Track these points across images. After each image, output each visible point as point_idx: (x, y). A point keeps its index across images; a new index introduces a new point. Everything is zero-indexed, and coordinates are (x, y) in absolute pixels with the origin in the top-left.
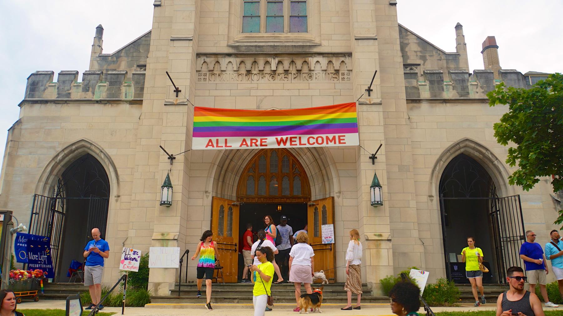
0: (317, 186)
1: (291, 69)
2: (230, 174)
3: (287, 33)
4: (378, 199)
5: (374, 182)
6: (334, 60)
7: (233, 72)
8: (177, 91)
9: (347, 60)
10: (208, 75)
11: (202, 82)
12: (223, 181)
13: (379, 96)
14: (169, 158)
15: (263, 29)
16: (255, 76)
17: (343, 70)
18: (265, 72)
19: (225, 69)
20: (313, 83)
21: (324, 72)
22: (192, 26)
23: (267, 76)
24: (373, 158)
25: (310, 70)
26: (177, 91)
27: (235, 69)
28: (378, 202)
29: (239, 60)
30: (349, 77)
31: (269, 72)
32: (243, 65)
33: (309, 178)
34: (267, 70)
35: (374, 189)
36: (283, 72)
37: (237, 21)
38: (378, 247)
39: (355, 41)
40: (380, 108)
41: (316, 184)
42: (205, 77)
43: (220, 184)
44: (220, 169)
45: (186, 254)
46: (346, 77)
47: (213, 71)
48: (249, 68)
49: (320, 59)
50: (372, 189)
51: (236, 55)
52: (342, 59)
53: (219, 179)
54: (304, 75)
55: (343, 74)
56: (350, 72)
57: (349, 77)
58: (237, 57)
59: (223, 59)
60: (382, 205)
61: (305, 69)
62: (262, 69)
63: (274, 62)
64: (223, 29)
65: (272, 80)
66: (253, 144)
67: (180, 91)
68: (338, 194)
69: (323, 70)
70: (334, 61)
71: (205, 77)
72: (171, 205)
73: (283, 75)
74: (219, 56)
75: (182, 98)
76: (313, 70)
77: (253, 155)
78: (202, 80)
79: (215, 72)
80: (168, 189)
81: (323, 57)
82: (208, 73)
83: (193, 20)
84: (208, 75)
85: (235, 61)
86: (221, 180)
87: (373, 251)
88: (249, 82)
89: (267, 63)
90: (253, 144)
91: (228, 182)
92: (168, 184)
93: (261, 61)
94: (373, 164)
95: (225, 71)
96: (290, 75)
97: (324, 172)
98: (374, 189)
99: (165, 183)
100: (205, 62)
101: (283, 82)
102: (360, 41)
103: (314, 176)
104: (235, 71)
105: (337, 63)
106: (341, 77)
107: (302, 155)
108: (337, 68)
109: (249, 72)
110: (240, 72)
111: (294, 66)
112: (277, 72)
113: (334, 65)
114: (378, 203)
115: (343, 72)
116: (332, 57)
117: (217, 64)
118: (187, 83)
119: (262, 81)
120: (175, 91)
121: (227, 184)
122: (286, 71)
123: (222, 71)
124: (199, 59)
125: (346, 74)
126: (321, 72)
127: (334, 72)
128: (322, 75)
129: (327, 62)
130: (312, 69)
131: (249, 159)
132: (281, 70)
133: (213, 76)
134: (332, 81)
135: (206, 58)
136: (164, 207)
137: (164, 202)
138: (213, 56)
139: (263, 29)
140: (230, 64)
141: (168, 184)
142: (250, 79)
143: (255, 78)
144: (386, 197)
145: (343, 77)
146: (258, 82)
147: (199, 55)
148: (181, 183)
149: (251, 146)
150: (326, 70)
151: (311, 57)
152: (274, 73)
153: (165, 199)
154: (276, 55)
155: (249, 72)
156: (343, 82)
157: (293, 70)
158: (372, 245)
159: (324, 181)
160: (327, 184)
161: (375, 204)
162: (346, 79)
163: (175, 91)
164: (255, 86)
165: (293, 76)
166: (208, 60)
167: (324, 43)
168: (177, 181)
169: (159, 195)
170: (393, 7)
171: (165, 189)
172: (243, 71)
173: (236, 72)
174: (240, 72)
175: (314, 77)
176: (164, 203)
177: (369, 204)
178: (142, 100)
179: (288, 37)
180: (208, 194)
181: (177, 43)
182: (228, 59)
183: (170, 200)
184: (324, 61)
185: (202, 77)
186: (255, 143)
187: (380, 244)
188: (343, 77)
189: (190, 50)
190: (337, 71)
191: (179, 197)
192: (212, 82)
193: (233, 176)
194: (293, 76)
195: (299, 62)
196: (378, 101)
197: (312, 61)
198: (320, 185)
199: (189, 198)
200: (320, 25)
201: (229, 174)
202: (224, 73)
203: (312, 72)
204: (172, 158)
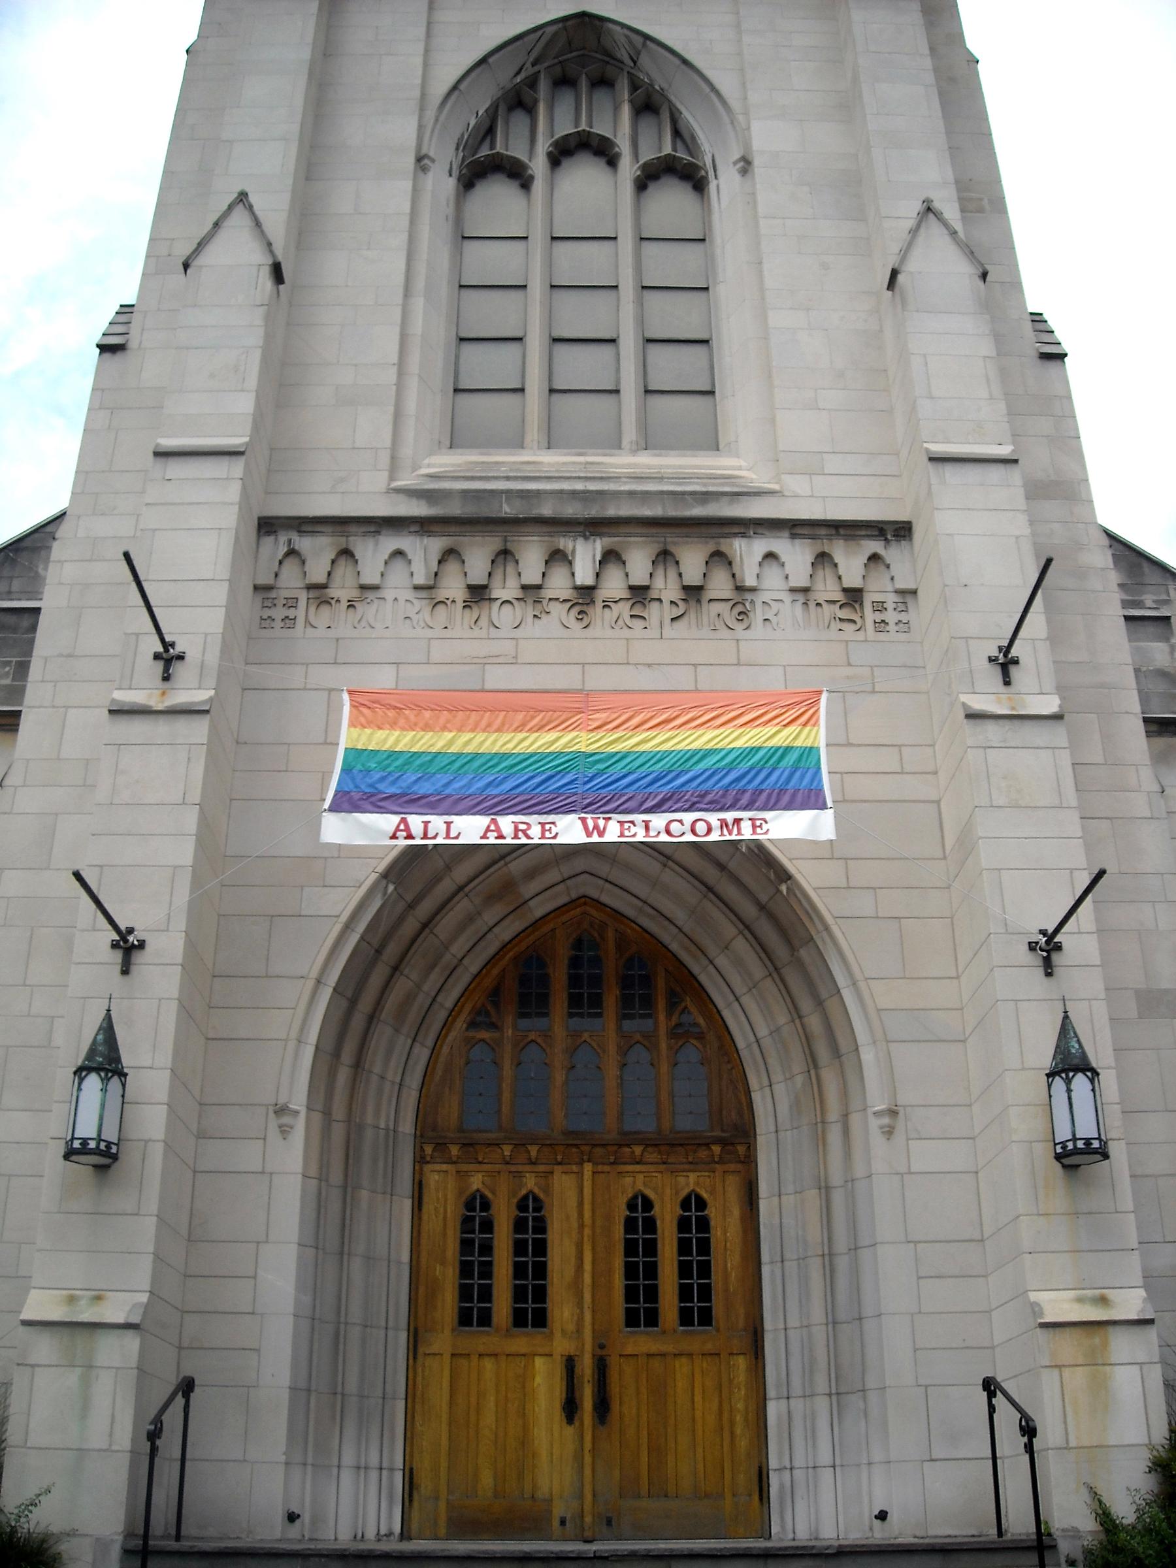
0: (779, 1089)
1: (659, 583)
2: (389, 1031)
3: (634, 452)
4: (1086, 1129)
5: (1062, 1049)
6: (839, 551)
7: (410, 594)
8: (168, 659)
9: (893, 554)
10: (302, 603)
11: (278, 631)
12: (358, 1065)
13: (1049, 684)
14: (115, 945)
15: (533, 433)
16: (507, 607)
17: (878, 589)
18: (548, 593)
19: (376, 580)
20: (756, 639)
21: (801, 598)
22: (245, 404)
23: (558, 610)
24: (1048, 949)
25: (740, 589)
26: (168, 659)
27: (420, 580)
28: (1088, 1142)
29: (436, 545)
30: (903, 617)
31: (567, 594)
32: (452, 567)
33: (744, 1054)
34: (559, 585)
35: (1068, 1082)
36: (625, 594)
37: (425, 403)
38: (1097, 1361)
39: (929, 464)
40: (1058, 735)
41: (777, 1076)
42: (291, 613)
43: (343, 1076)
44: (344, 1004)
45: (180, 1401)
46: (891, 616)
47: (324, 587)
48: (478, 578)
49: (781, 545)
50: (1058, 1083)
51: (423, 526)
52: (875, 546)
53: (337, 1054)
54: (717, 608)
55: (880, 607)
56: (909, 599)
57: (903, 617)
58: (430, 534)
59: (370, 542)
60: (1106, 1156)
61: (720, 585)
62: (537, 580)
63: (585, 556)
64: (371, 426)
65: (576, 626)
66: (520, 834)
67: (181, 657)
68: (886, 1120)
69: (793, 590)
70: (838, 557)
71: (291, 613)
72: (115, 1157)
73: (624, 609)
74: (353, 528)
75: (190, 690)
76: (753, 590)
77: (492, 950)
78: (278, 624)
79: (333, 592)
80: (106, 1081)
81: (793, 536)
82: (303, 596)
83: (252, 382)
84: (302, 603)
85: (422, 551)
86: (347, 1057)
87: (1077, 1378)
88: (476, 632)
89: (557, 557)
90: (520, 834)
91: (377, 1069)
92: (105, 1060)
93: (531, 559)
94: (1049, 974)
95: (376, 588)
96: (655, 606)
97: (814, 1022)
98: (1068, 1082)
99: (92, 1052)
100: (292, 552)
101: (626, 633)
102: (949, 469)
103: (767, 1042)
104: (417, 588)
105: (851, 564)
106: (870, 616)
107: (712, 951)
108: (853, 579)
109: (478, 594)
110: (441, 594)
111: (672, 574)
112: (602, 594)
113: (841, 571)
114: (1088, 1150)
115: (879, 597)
116: (830, 537)
117: (342, 562)
118: (213, 621)
119: (532, 629)
120: (157, 657)
121: (374, 1079)
122: (640, 594)
123: (363, 587)
124: (268, 541)
125: (890, 606)
126: (787, 597)
127: (839, 596)
128: (790, 611)
129: (809, 558)
130: (750, 581)
131: (474, 969)
132: (614, 585)
133: (325, 609)
134: (833, 634)
135: (295, 536)
136: (81, 1170)
137: (85, 1142)
138: (328, 529)
139: (533, 433)
140: (399, 564)
141: (105, 1060)
142: (484, 621)
143: (505, 616)
144: (1114, 1128)
145: (879, 617)
146: (518, 633)
147: (267, 526)
148: (165, 1058)
149: (516, 837)
150: (806, 590)
151: (743, 535)
152: (585, 596)
153: (87, 1129)
154: (593, 527)
155: (478, 594)
156: (882, 636)
157: (667, 587)
158: (1068, 1346)
159: (813, 1061)
160: (829, 1078)
161: (1076, 1151)
162: (892, 627)
163: (157, 657)
164: (508, 647)
165: (669, 612)
166: (304, 544)
167: (796, 484)
168: (148, 1053)
169: (61, 1111)
170: (1052, 365)
171: (93, 1082)
172: (453, 587)
173: (424, 594)
174: (441, 594)
175: (758, 614)
176: (84, 1150)
177: (1044, 1154)
178: (18, 714)
179: (636, 468)
180: (286, 1120)
181: (176, 469)
182: (390, 542)
183: (110, 1134)
184: (797, 557)
185: (279, 613)
186: (524, 832)
187: (1105, 1344)
188: (879, 617)
189: (233, 492)
190: (854, 596)
191: (152, 1122)
192: (321, 632)
193: (403, 1042)
194: (669, 612)
195: (692, 560)
196: (1050, 705)
197: (748, 552)
198: (799, 1080)
199: (201, 1135)
200: (773, 421)
201: (383, 1033)
202: (371, 595)
203: (749, 596)
204: (128, 947)
